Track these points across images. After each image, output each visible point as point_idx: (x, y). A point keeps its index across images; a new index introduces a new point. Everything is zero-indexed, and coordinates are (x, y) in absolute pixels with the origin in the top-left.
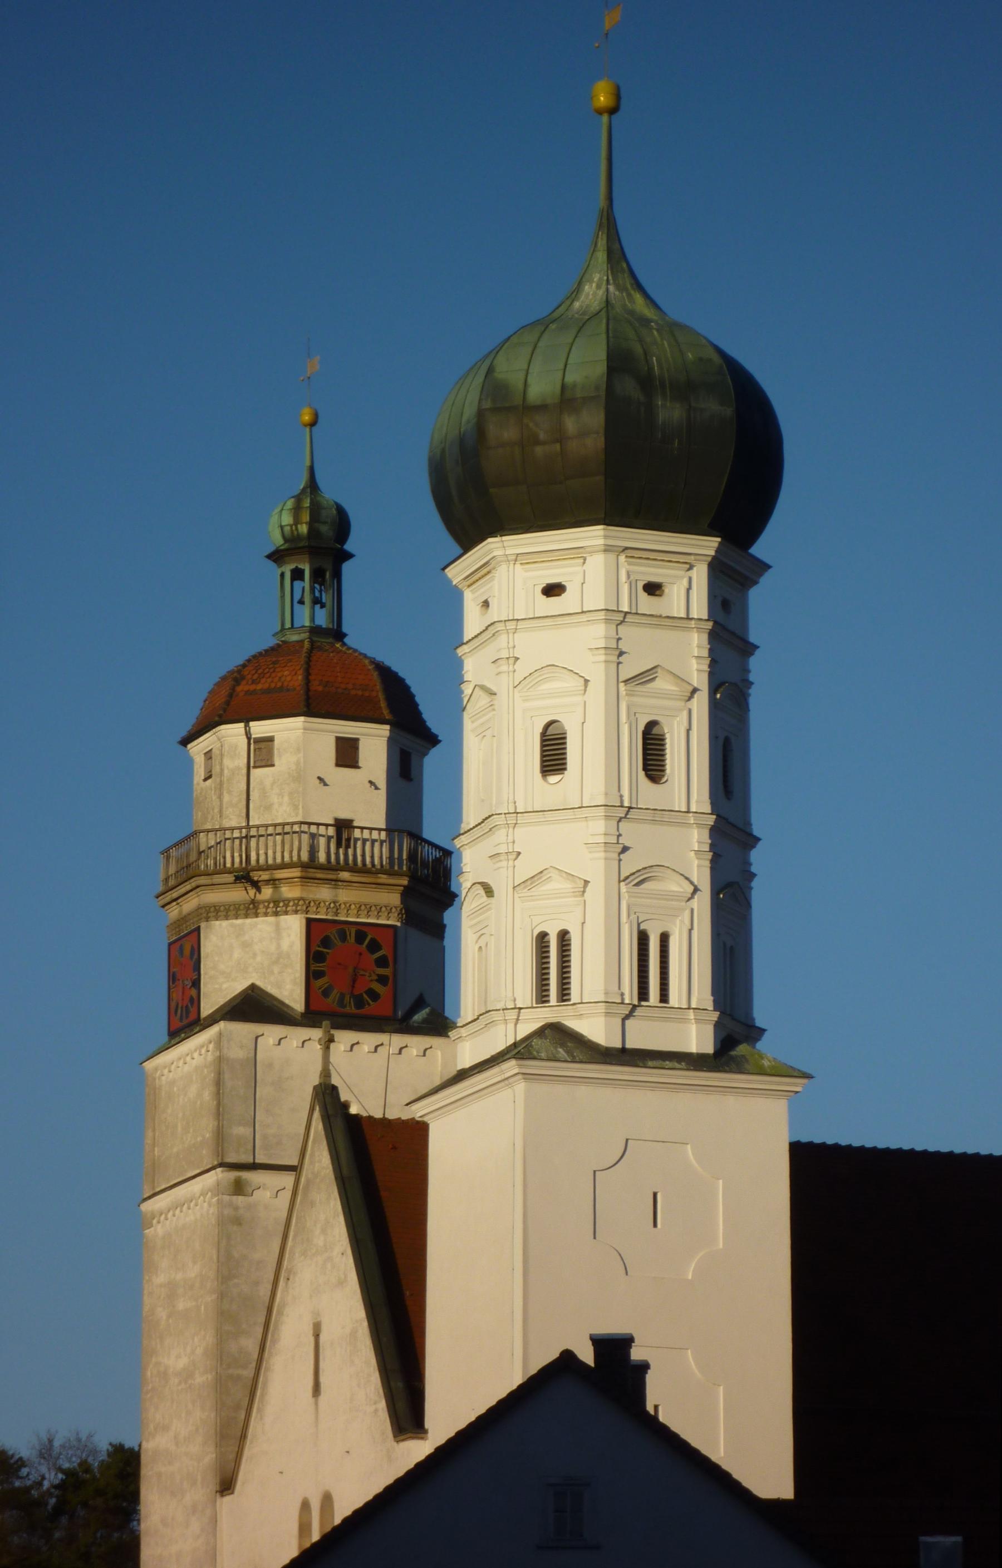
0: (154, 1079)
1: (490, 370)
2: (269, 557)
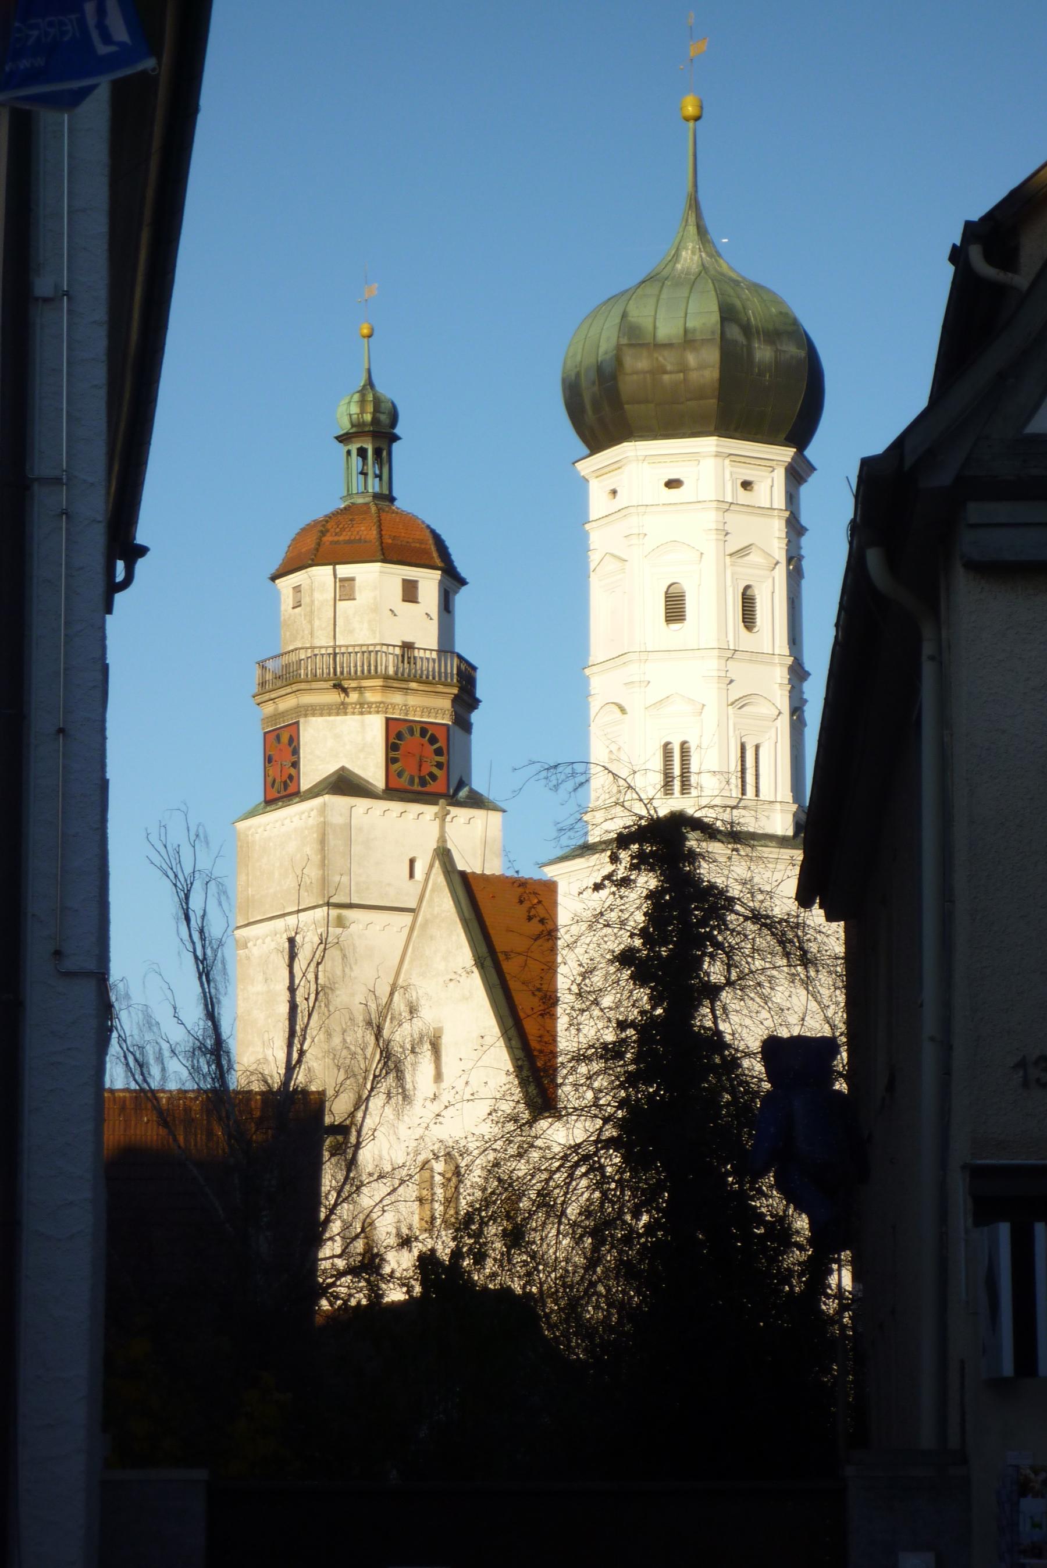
0: (247, 836)
1: (624, 315)
2: (337, 438)
